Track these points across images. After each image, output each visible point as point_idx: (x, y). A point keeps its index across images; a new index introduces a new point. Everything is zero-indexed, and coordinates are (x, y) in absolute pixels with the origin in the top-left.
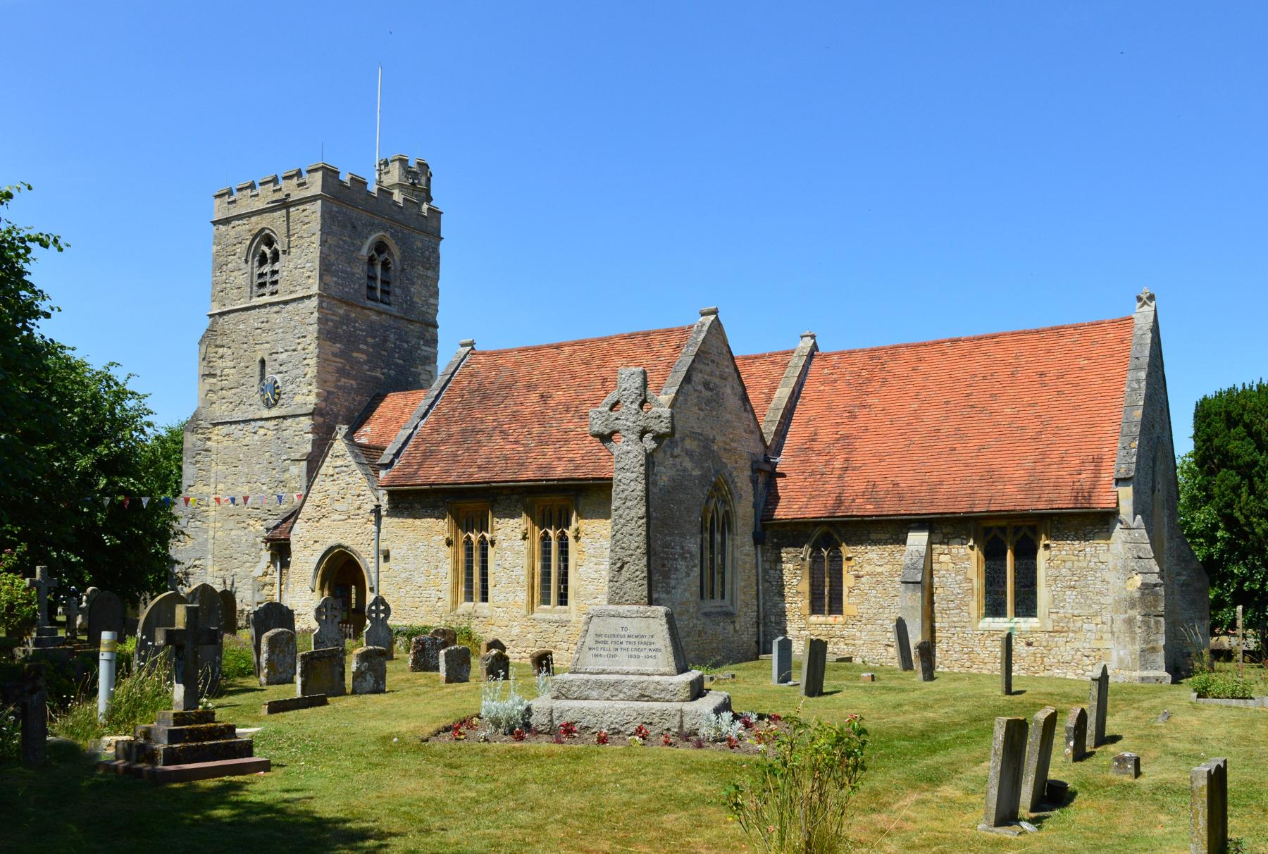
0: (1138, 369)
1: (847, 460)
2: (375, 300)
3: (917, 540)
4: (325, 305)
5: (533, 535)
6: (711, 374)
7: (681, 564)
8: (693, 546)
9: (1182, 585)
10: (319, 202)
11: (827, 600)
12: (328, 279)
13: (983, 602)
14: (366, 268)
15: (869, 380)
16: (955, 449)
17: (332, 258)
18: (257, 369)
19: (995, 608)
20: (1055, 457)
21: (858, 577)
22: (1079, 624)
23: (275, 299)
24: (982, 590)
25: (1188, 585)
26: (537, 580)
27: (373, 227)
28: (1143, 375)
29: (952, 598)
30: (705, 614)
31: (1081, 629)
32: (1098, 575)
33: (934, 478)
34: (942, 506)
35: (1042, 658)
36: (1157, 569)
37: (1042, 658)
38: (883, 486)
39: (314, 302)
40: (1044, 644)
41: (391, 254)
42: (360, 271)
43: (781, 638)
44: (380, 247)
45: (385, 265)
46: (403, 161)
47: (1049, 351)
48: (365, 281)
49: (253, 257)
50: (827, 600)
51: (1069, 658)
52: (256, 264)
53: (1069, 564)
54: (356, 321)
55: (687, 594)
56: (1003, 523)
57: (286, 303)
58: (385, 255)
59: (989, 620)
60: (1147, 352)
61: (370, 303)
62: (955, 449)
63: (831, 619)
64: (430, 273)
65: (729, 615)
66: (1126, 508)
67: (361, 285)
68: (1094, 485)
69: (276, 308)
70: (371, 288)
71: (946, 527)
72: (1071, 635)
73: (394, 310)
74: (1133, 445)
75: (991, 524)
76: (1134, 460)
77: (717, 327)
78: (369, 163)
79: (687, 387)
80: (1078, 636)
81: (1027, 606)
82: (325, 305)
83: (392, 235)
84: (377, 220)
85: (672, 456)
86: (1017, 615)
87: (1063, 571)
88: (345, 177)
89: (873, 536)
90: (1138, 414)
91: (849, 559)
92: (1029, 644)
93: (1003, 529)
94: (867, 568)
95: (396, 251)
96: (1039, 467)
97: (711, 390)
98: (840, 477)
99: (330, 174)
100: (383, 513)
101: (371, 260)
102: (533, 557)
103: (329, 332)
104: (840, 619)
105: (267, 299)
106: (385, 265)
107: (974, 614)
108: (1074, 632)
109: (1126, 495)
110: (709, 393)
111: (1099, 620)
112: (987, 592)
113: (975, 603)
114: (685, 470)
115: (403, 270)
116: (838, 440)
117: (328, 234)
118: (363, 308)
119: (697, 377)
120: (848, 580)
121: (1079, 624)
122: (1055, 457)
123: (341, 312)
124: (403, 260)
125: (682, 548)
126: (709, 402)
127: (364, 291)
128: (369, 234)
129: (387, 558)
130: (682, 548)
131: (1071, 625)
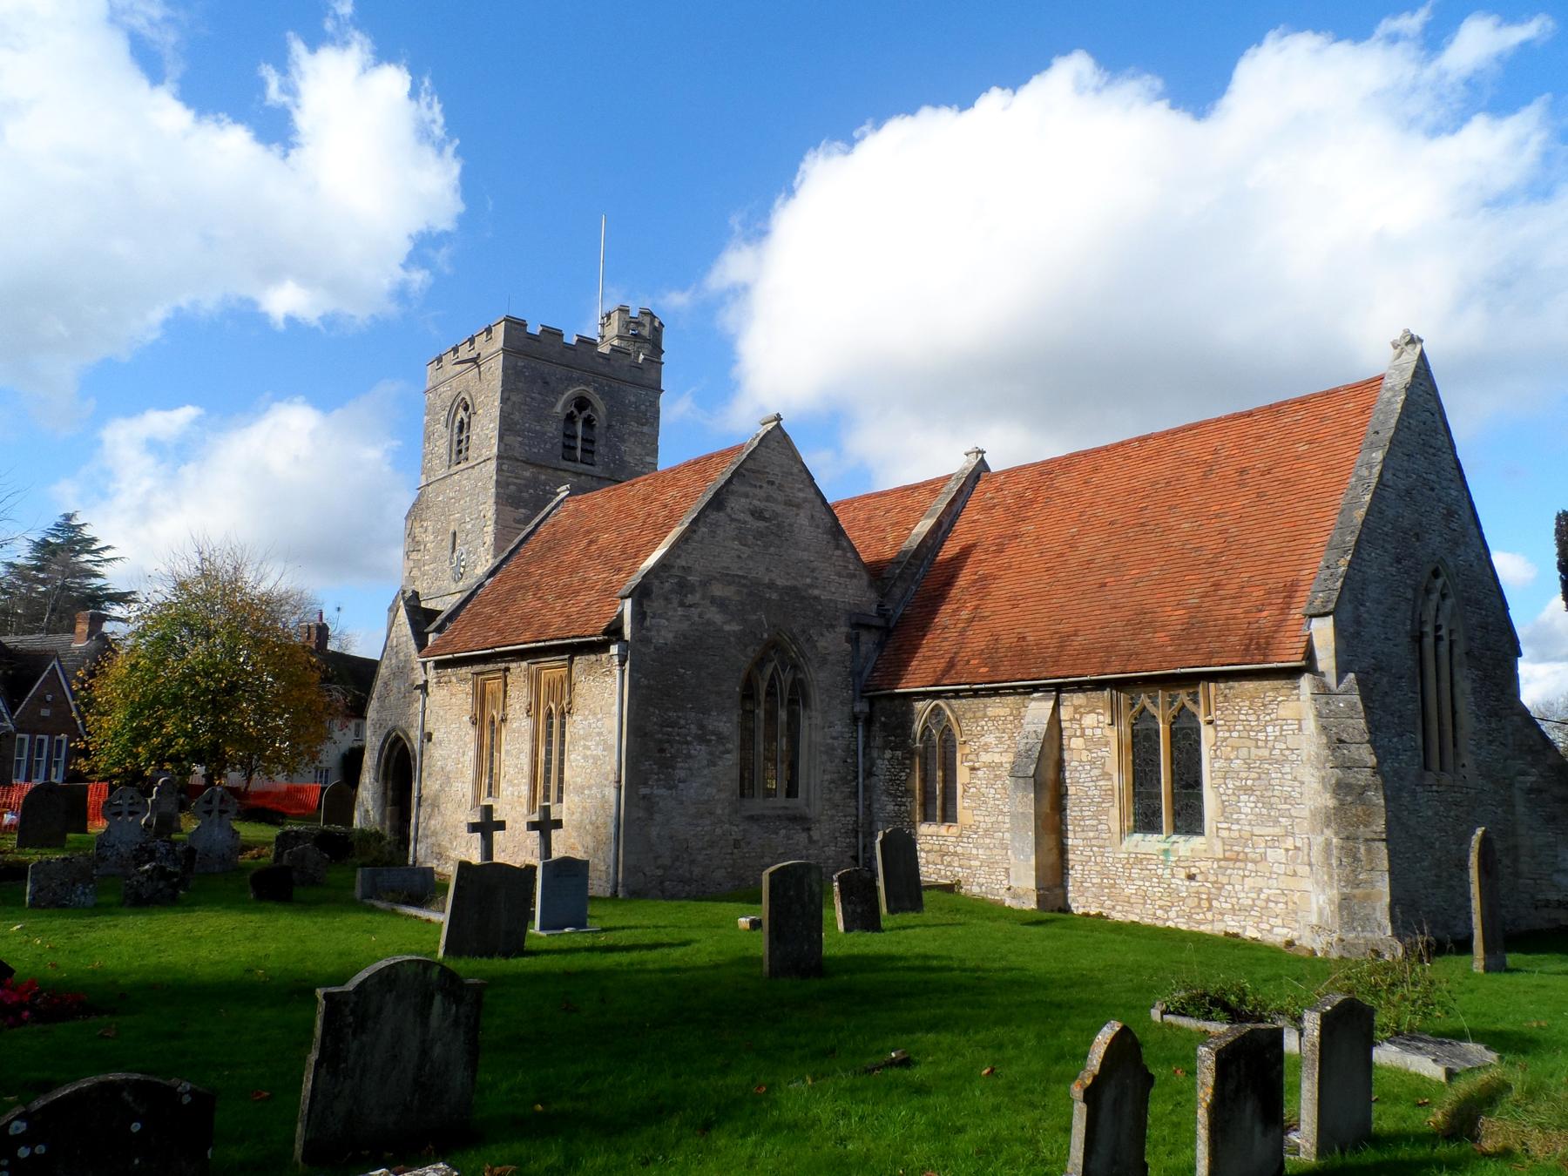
0: (1373, 446)
1: (976, 607)
2: (575, 460)
4: (505, 467)
6: (768, 499)
7: (699, 750)
8: (726, 724)
9: (1531, 791)
11: (939, 802)
12: (509, 439)
13: (1129, 809)
14: (561, 425)
15: (1032, 501)
16: (1105, 585)
17: (517, 416)
20: (1230, 589)
21: (973, 769)
24: (1128, 791)
25: (1540, 791)
26: (541, 769)
27: (571, 381)
28: (1378, 456)
30: (751, 818)
31: (1264, 857)
32: (1287, 769)
33: (1064, 628)
35: (1209, 900)
36: (1372, 760)
37: (1209, 900)
38: (1008, 640)
39: (492, 465)
40: (1212, 878)
41: (594, 410)
42: (553, 429)
44: (582, 403)
45: (588, 422)
46: (623, 310)
47: (1260, 438)
48: (559, 440)
50: (939, 802)
53: (1244, 753)
54: (545, 484)
55: (712, 791)
58: (588, 412)
59: (1138, 836)
60: (1393, 422)
61: (565, 464)
62: (1105, 585)
63: (943, 830)
64: (645, 429)
65: (800, 821)
67: (554, 445)
68: (1279, 625)
70: (569, 449)
72: (1250, 866)
73: (597, 470)
74: (1342, 562)
76: (1339, 584)
78: (592, 321)
79: (714, 516)
80: (1260, 867)
82: (505, 467)
83: (596, 389)
84: (576, 374)
85: (682, 604)
86: (1176, 830)
87: (1237, 764)
90: (1359, 514)
92: (1191, 877)
94: (985, 757)
95: (600, 406)
96: (1208, 603)
97: (765, 519)
98: (962, 633)
99: (515, 326)
101: (570, 418)
103: (509, 496)
104: (954, 830)
106: (588, 422)
107: (1116, 827)
108: (1255, 862)
109: (1323, 633)
110: (762, 524)
111: (1289, 843)
112: (1136, 794)
113: (1114, 815)
114: (709, 623)
115: (609, 427)
116: (975, 581)
117: (512, 390)
118: (556, 469)
119: (736, 504)
122: (1230, 589)
123: (527, 474)
124: (610, 414)
125: (701, 727)
126: (759, 535)
127: (559, 450)
128: (566, 389)
129: (430, 740)
130: (701, 727)
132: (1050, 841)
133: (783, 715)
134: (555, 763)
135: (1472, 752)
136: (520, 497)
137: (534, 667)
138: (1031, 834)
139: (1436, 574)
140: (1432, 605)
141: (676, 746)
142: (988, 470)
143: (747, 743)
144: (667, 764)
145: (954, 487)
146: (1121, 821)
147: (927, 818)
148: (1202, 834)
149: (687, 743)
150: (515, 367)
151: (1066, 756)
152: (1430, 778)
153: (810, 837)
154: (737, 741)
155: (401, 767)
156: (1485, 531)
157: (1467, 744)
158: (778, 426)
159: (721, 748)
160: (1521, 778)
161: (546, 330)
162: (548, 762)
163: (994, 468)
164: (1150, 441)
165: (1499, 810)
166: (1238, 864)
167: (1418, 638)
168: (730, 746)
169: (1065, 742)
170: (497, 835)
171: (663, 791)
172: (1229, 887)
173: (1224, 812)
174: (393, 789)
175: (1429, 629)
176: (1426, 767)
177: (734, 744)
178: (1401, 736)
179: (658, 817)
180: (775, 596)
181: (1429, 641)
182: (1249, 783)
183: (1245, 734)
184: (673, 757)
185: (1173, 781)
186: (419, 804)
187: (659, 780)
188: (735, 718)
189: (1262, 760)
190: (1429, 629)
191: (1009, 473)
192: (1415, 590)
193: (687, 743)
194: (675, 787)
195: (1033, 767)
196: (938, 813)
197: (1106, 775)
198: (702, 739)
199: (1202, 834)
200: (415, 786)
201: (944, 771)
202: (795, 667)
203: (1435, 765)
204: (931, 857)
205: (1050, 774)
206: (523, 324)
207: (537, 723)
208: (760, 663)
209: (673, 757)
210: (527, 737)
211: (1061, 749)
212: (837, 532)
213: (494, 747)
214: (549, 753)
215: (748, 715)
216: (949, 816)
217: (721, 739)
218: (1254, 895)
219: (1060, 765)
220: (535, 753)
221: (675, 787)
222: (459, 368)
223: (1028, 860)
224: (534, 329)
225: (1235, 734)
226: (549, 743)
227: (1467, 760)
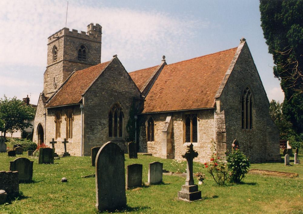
3: (168, 119)
5: (67, 119)
7: (100, 127)
8: (105, 121)
10: (64, 37)
11: (151, 137)
12: (66, 56)
13: (185, 138)
18: (53, 79)
19: (188, 140)
22: (206, 145)
23: (57, 62)
24: (185, 134)
29: (177, 136)
31: (207, 146)
34: (175, 108)
39: (62, 63)
43: (232, 148)
49: (54, 52)
50: (151, 137)
51: (204, 156)
52: (54, 54)
56: (189, 113)
57: (58, 63)
59: (187, 143)
66: (218, 108)
69: (56, 64)
71: (175, 115)
72: (205, 148)
75: (187, 113)
77: (246, 47)
80: (206, 148)
81: (195, 140)
87: (203, 128)
88: (71, 30)
89: (161, 118)
91: (155, 125)
93: (189, 115)
100: (47, 115)
102: (67, 125)
104: (60, 138)
105: (56, 62)
108: (205, 147)
109: (218, 103)
120: (155, 131)
121: (206, 145)
130: (100, 122)
131: (205, 145)
132: (170, 145)
133: (118, 119)
134: (249, 120)
135: (255, 125)
136: (67, 70)
137: (66, 110)
138: (166, 143)
139: (247, 88)
140: (246, 96)
141: (94, 126)
142: (167, 64)
143: (110, 126)
144: (93, 130)
145: (159, 68)
146: (183, 140)
147: (149, 140)
148: (197, 142)
149: (97, 125)
150: (67, 39)
151: (174, 127)
152: (243, 130)
153: (125, 145)
154: (108, 125)
155: (41, 131)
156: (261, 79)
157: (254, 123)
158: (117, 57)
159: (104, 126)
160: (268, 130)
161: (74, 30)
162: (70, 130)
163: (168, 64)
164: (196, 59)
165: (262, 136)
166: (203, 148)
167: (243, 102)
168: (106, 126)
169: (174, 124)
170: (55, 144)
171: (92, 136)
172: (201, 153)
173: (200, 138)
174: (40, 136)
175: (245, 100)
176: (243, 128)
177: (107, 126)
178: (236, 122)
179: (91, 141)
180: (116, 94)
181: (245, 103)
182: (205, 132)
183: (204, 122)
184: (94, 128)
185: (193, 132)
186: (45, 139)
187: (91, 133)
188: (107, 120)
189: (207, 127)
190: (245, 100)
191: (170, 65)
192: (241, 92)
193: (97, 125)
194: (94, 135)
195: (166, 130)
196: (151, 139)
197: (181, 131)
198: (100, 125)
199: (197, 142)
200: (44, 135)
201: (152, 130)
202: (121, 109)
203: (249, 127)
204: (150, 148)
205: (170, 131)
206: (68, 29)
207: (67, 122)
208: (113, 109)
209: (94, 128)
210: (66, 125)
211: (173, 126)
212: (130, 79)
213: (60, 127)
214: (70, 128)
215: (110, 120)
216: (153, 139)
217: (104, 124)
218: (205, 154)
219: (173, 129)
220: (67, 128)
221: (94, 135)
222: (55, 39)
223: (165, 148)
224: (71, 30)
225: (203, 122)
226: (70, 126)
227: (254, 127)
